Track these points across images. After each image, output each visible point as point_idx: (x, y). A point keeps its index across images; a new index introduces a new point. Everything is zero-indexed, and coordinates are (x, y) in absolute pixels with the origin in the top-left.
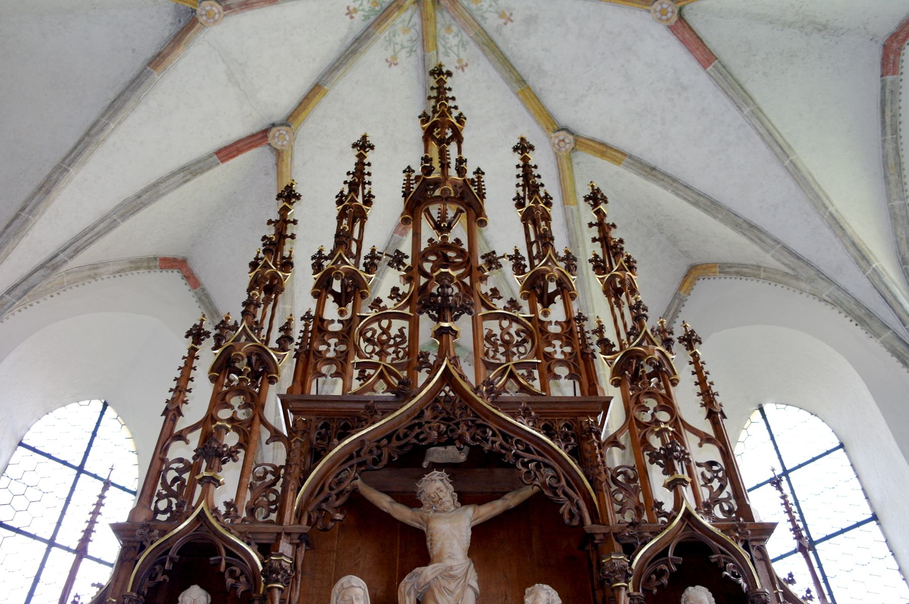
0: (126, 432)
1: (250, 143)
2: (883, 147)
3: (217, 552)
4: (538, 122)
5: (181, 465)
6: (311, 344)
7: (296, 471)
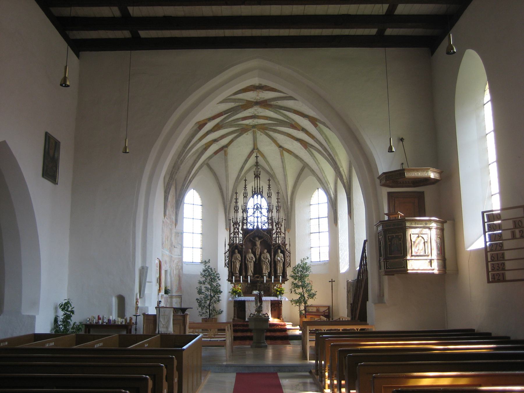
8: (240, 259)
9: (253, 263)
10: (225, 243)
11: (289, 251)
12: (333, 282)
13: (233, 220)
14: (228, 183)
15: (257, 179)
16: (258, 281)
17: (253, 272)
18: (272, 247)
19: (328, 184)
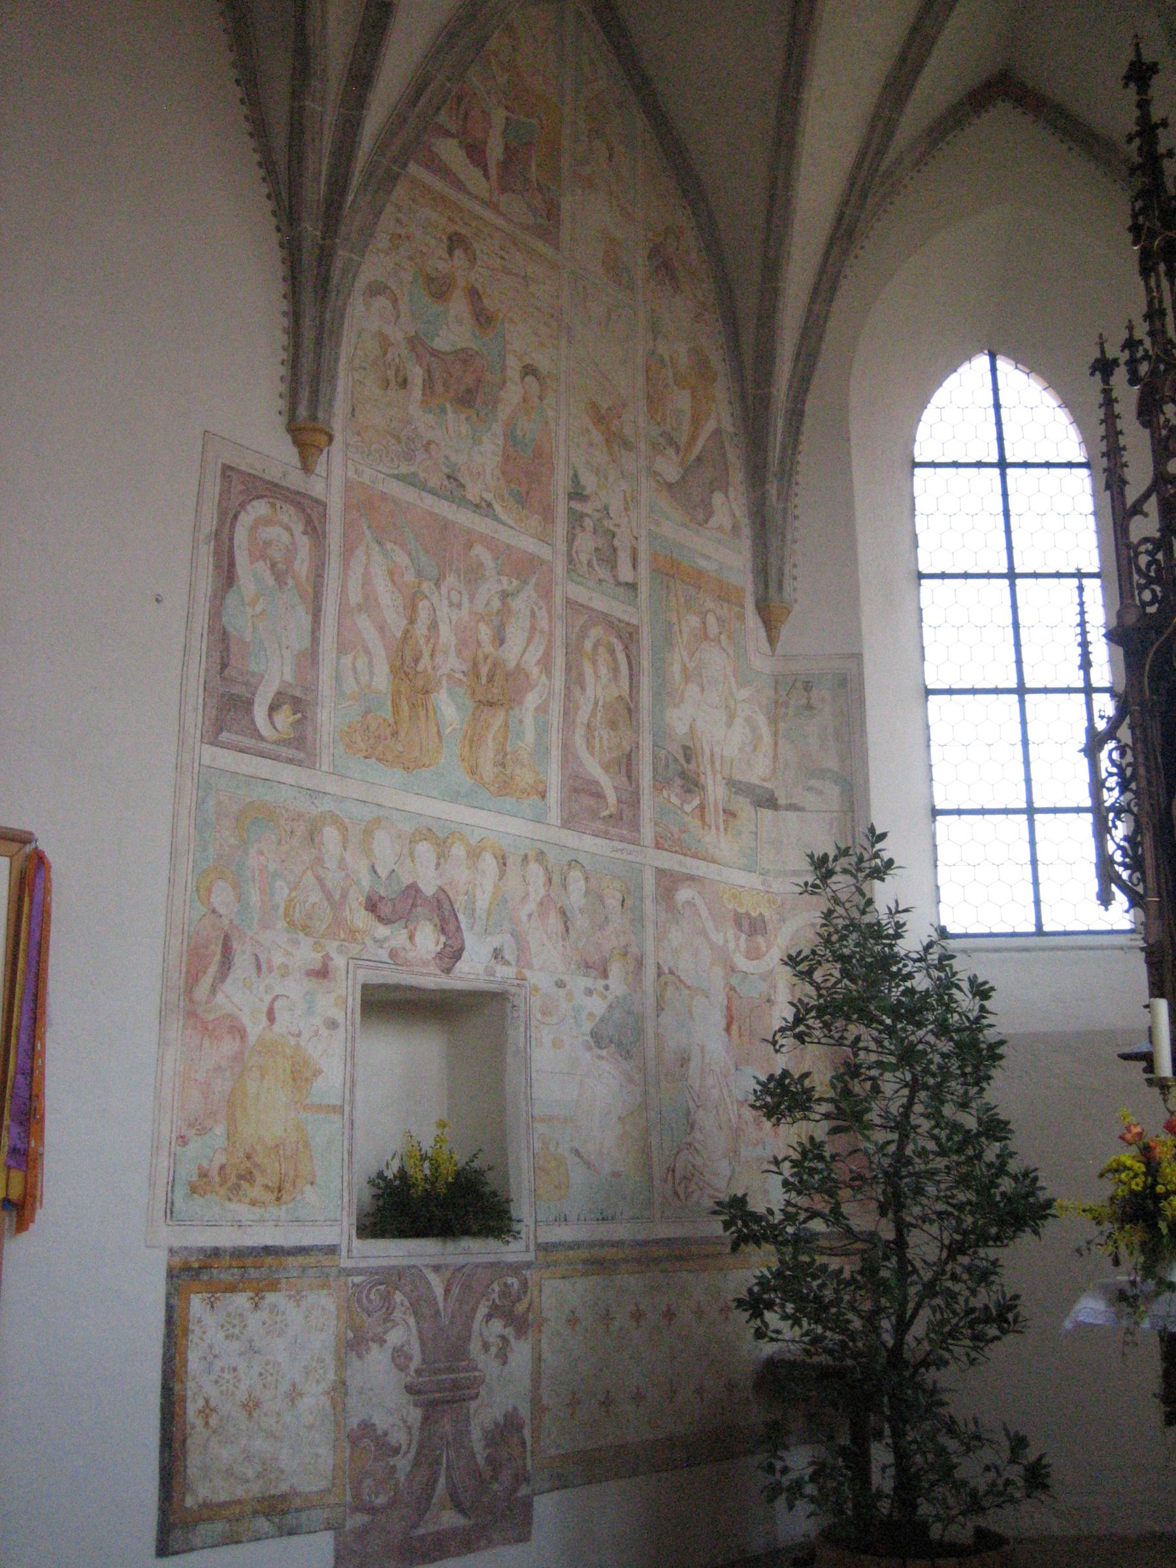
5: (1150, 546)
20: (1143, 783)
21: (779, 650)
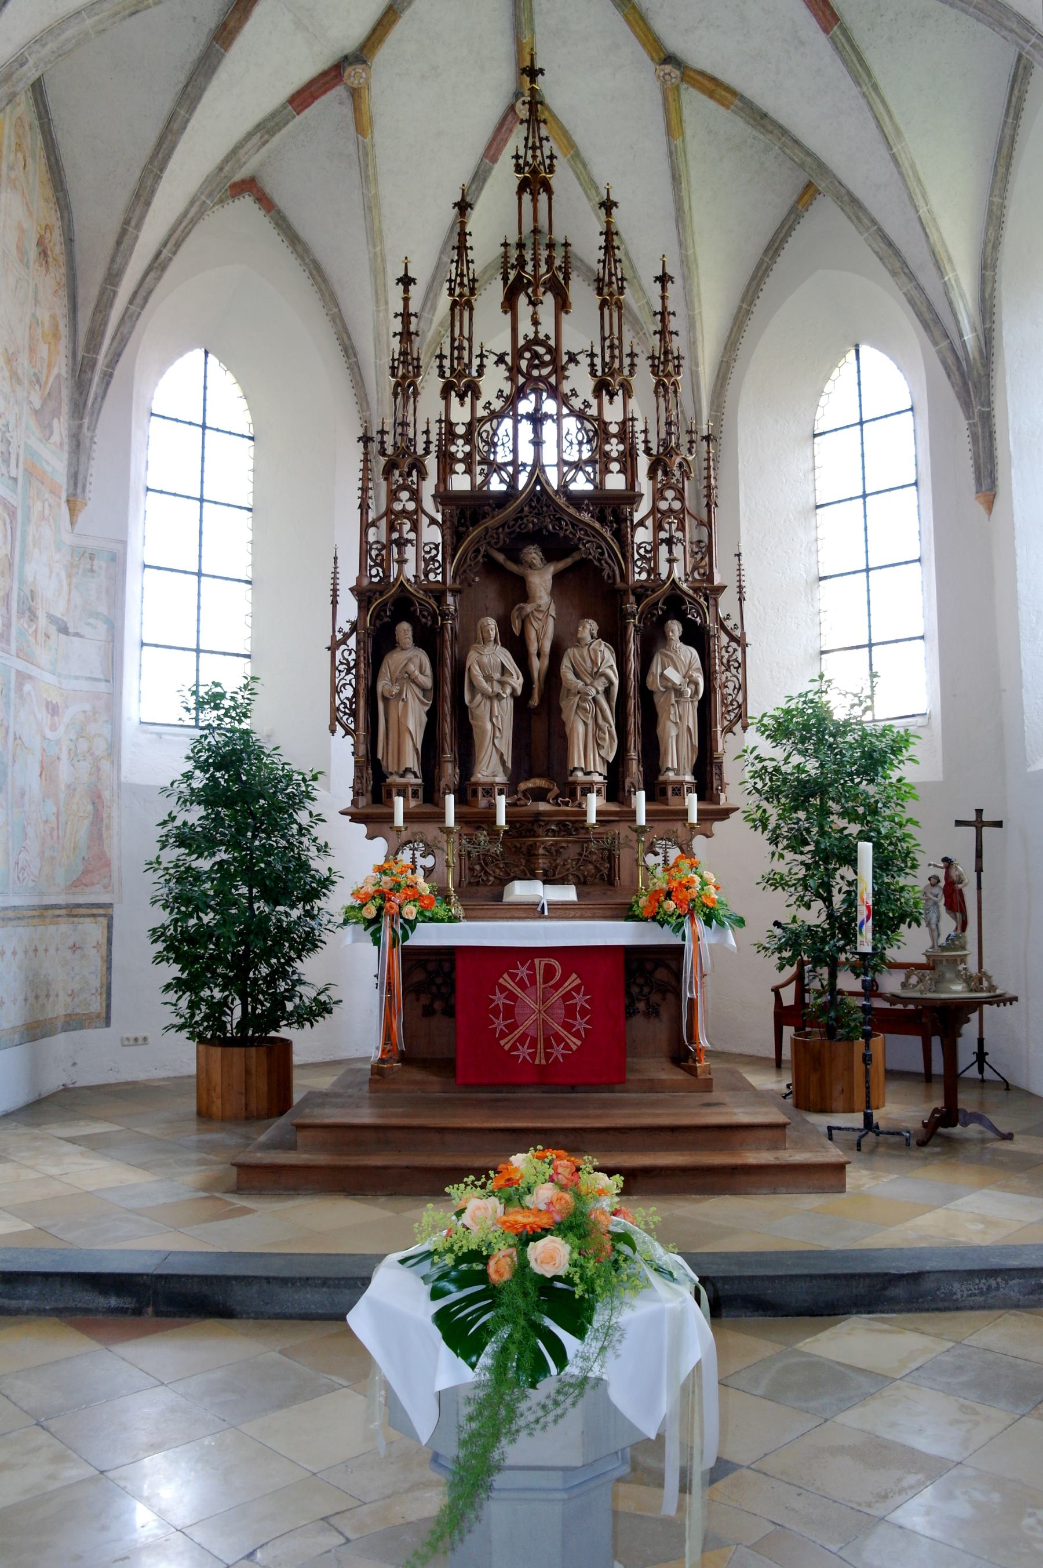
0: (230, 378)
1: (324, 84)
2: (1003, 130)
3: (413, 604)
4: (644, 45)
5: (379, 546)
6: (445, 445)
7: (449, 549)
8: (427, 681)
9: (508, 705)
10: (335, 584)
11: (737, 633)
12: (986, 831)
13: (382, 443)
14: (382, 308)
15: (535, 201)
16: (540, 813)
17: (509, 764)
18: (631, 606)
19: (948, 267)
20: (362, 672)
21: (77, 527)
